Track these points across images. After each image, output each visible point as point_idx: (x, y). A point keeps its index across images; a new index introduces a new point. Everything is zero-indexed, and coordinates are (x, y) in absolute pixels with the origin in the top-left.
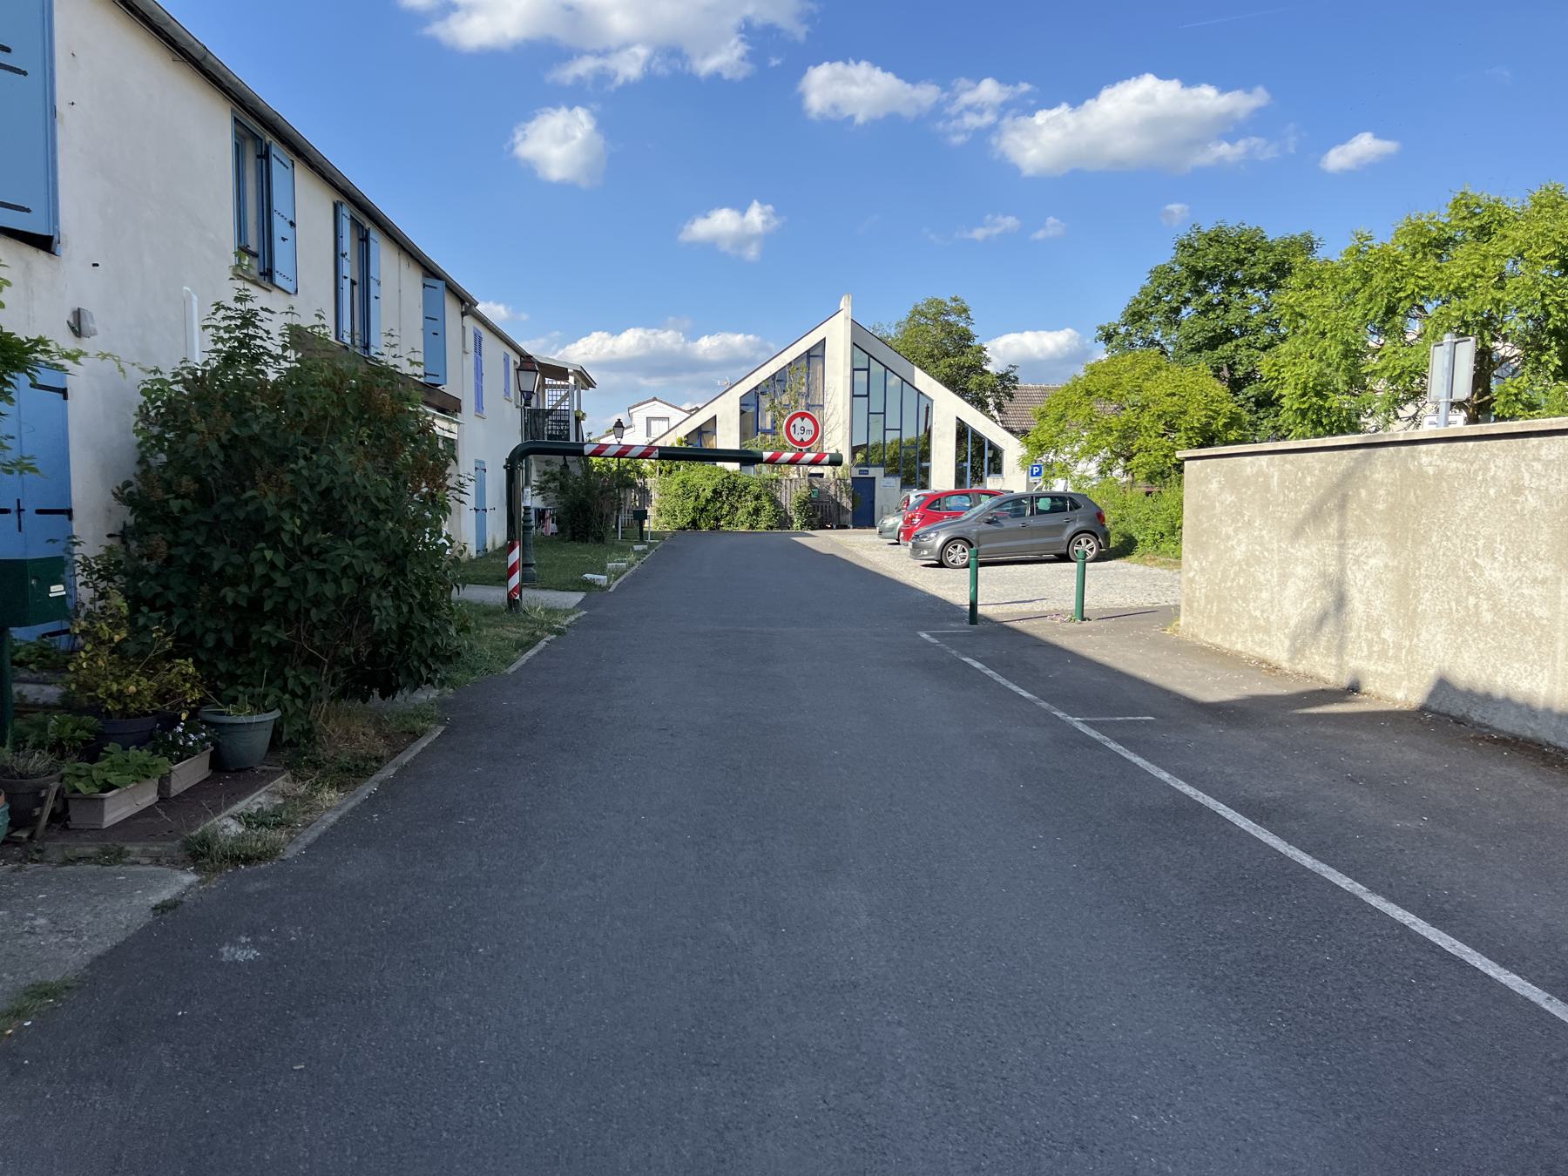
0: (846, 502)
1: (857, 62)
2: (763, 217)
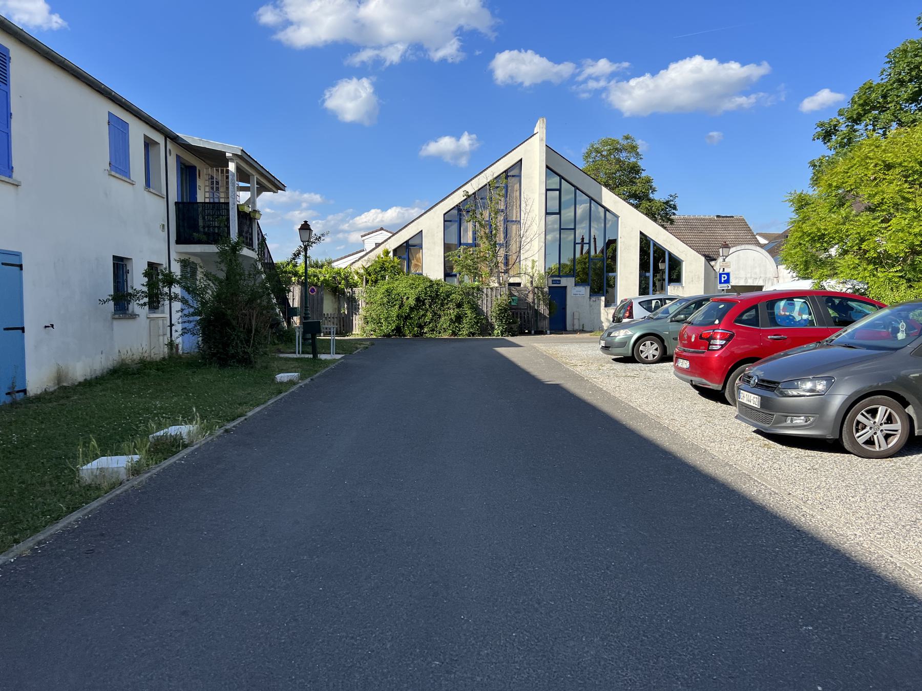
0: (543, 309)
1: (526, 51)
2: (470, 142)
